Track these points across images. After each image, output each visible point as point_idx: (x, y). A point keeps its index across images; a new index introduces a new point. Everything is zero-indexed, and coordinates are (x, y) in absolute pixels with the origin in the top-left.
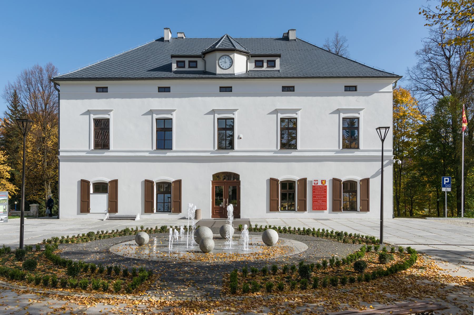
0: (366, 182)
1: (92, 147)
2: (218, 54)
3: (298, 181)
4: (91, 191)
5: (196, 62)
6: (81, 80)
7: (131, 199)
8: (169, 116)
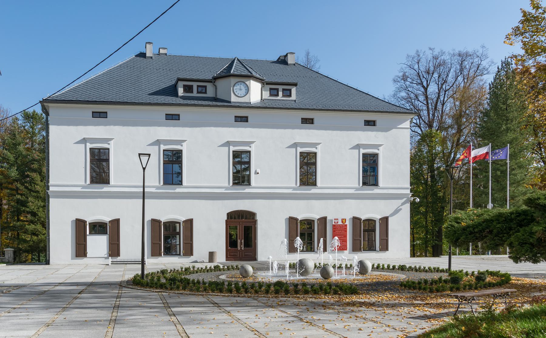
0: (385, 221)
1: (88, 182)
2: (233, 80)
3: (183, 222)
4: (88, 233)
5: (205, 87)
6: (77, 103)
7: (132, 242)
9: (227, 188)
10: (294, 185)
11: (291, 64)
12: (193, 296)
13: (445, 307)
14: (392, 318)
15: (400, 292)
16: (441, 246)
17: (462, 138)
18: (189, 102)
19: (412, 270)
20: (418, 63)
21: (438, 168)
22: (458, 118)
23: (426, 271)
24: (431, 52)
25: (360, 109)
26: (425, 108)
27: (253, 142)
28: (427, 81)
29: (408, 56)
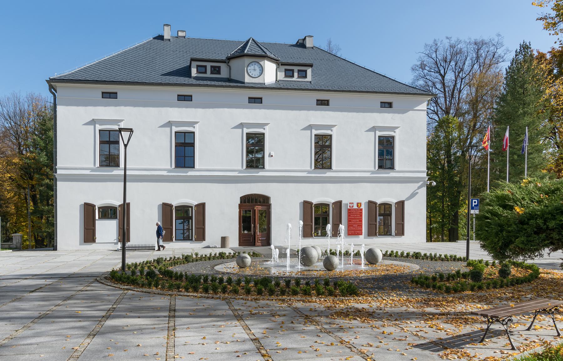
0: (401, 205)
2: (247, 60)
3: (195, 206)
5: (219, 67)
6: (85, 83)
7: (144, 225)
8: (190, 129)
9: (240, 172)
10: (309, 168)
11: (309, 47)
12: (158, 296)
13: (466, 322)
14: (392, 345)
15: (409, 292)
16: (457, 230)
17: (478, 124)
18: (201, 82)
19: (427, 258)
20: (436, 52)
21: (455, 154)
22: (474, 103)
23: (442, 260)
24: (448, 41)
25: (376, 90)
26: (442, 95)
27: (267, 124)
28: (445, 70)
29: (426, 45)
